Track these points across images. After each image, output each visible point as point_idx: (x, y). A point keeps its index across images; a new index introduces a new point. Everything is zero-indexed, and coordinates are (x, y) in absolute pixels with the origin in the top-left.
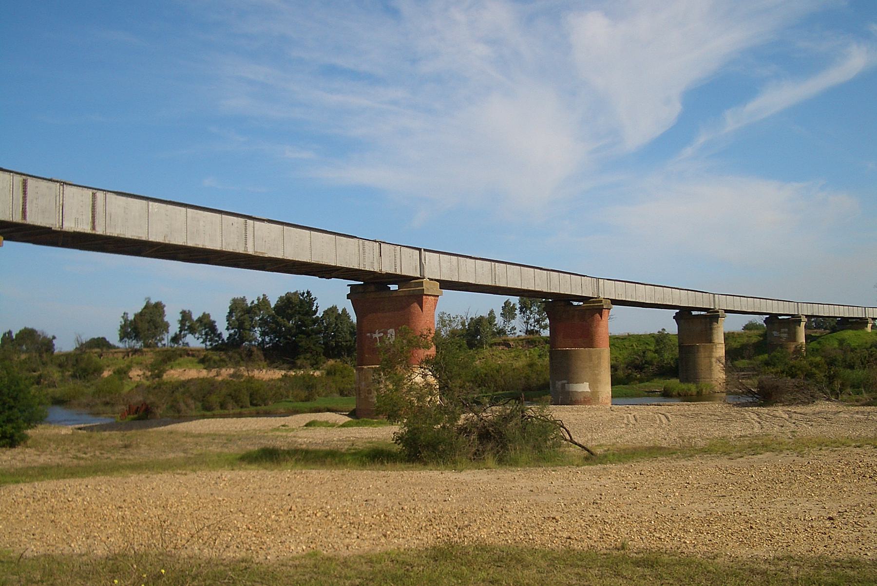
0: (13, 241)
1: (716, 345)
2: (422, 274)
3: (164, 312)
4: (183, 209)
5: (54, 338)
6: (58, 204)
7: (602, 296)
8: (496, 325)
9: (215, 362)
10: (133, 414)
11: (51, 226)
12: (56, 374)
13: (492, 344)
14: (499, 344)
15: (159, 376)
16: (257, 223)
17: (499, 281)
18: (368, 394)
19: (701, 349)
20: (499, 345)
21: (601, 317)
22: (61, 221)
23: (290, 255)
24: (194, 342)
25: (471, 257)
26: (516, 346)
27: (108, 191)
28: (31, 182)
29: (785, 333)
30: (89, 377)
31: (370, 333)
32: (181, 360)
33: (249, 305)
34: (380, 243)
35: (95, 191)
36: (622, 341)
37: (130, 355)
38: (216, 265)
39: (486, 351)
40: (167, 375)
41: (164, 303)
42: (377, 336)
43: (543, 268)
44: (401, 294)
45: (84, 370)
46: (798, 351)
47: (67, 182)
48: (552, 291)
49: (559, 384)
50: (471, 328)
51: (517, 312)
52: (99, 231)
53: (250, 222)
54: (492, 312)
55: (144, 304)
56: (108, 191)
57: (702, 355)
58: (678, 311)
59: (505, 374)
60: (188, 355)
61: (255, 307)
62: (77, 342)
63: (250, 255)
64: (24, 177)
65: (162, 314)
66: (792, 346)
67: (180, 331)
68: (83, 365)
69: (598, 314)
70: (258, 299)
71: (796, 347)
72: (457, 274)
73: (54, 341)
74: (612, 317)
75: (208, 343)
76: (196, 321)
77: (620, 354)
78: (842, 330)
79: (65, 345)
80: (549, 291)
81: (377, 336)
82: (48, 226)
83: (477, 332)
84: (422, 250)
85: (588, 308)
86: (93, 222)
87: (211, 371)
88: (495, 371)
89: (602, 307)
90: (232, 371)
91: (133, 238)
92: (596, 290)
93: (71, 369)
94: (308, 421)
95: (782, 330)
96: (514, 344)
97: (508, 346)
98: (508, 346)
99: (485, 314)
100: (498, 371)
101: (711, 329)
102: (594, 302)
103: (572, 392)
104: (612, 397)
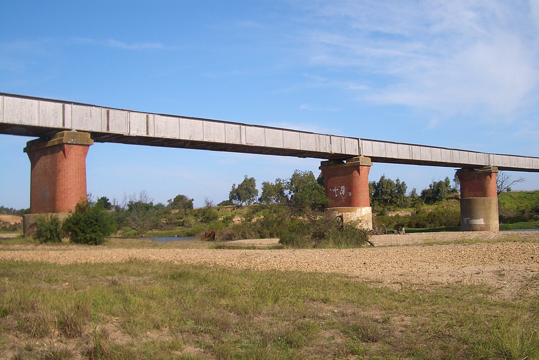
0: (4, 134)
2: (360, 154)
4: (201, 121)
5: (193, 200)
6: (127, 122)
7: (492, 165)
8: (450, 186)
10: (207, 238)
11: (123, 134)
12: (192, 220)
13: (448, 198)
14: (452, 198)
16: (247, 127)
17: (415, 157)
20: (452, 199)
22: (129, 131)
23: (185, 136)
25: (394, 143)
27: (155, 114)
28: (111, 111)
30: (210, 222)
34: (330, 136)
35: (148, 114)
36: (531, 195)
37: (235, 209)
38: (152, 146)
39: (444, 203)
42: (335, 190)
43: (447, 148)
44: (347, 165)
45: (208, 218)
47: (131, 110)
48: (454, 162)
49: (465, 220)
50: (435, 188)
52: (151, 135)
53: (243, 127)
54: (447, 178)
56: (155, 114)
59: (447, 216)
62: (206, 202)
63: (243, 145)
64: (107, 109)
65: (253, 185)
68: (207, 215)
72: (385, 153)
73: (193, 202)
77: (529, 203)
79: (198, 204)
80: (452, 162)
81: (335, 190)
82: (121, 134)
83: (438, 191)
84: (360, 139)
85: (482, 172)
86: (147, 131)
88: (440, 214)
91: (171, 138)
92: (487, 160)
93: (201, 218)
99: (443, 180)
100: (442, 214)
102: (486, 169)
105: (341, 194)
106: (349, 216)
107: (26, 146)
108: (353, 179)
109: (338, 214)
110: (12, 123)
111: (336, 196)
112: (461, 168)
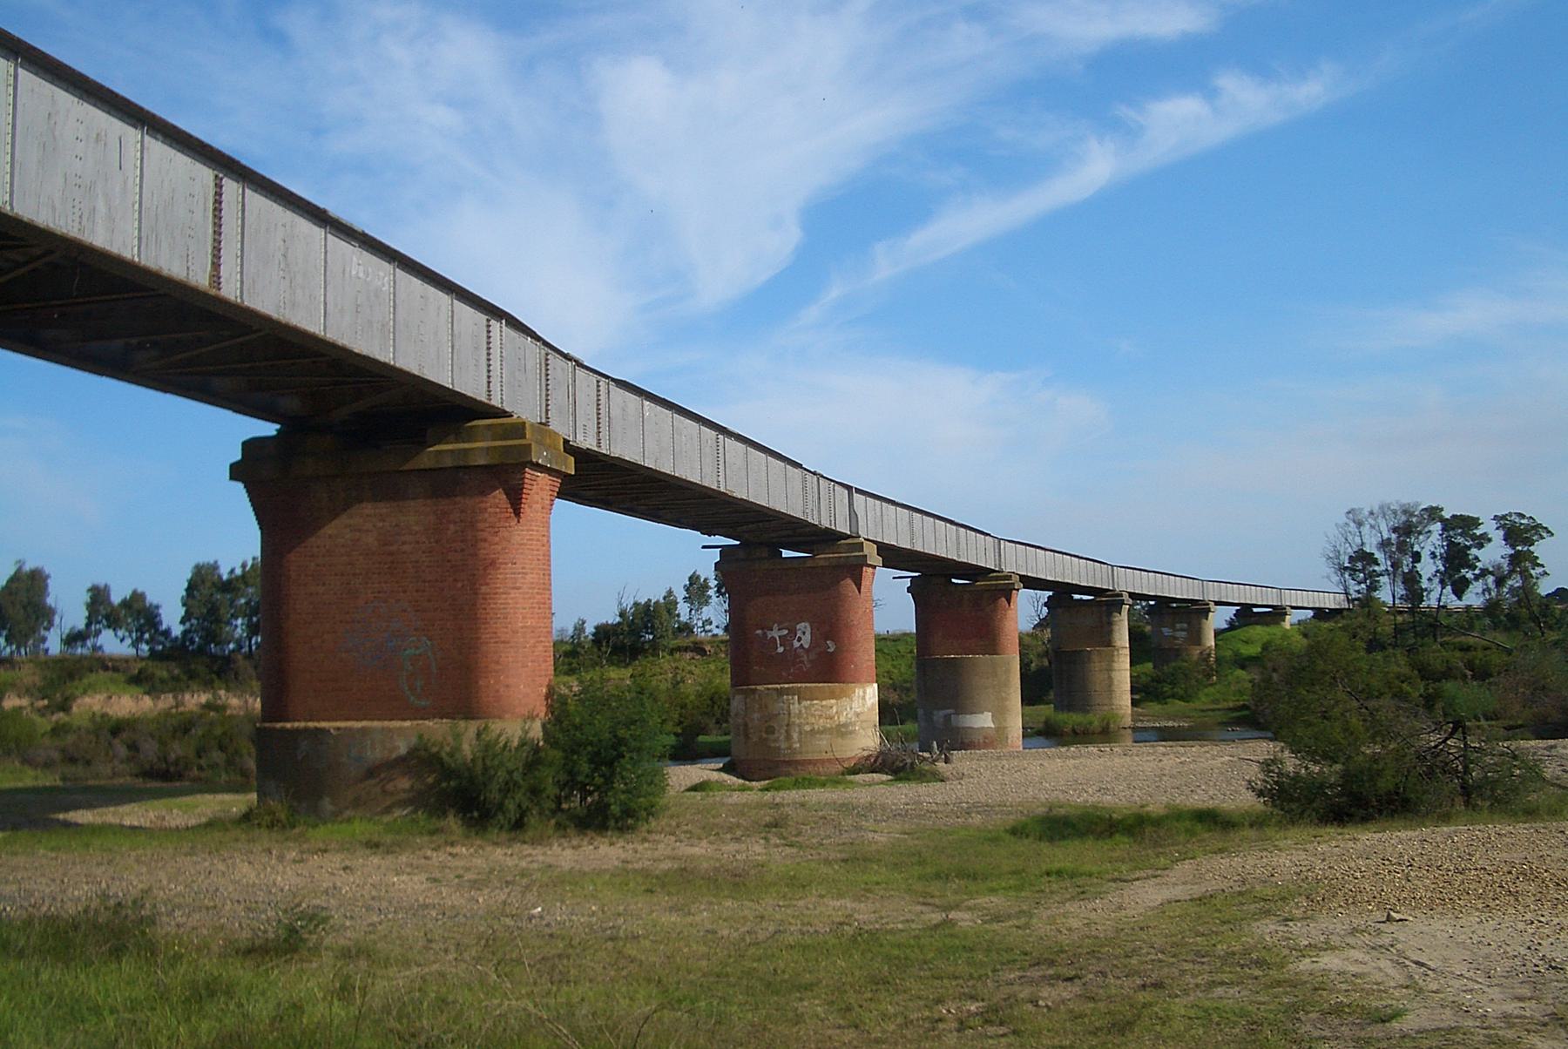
1: (1118, 650)
2: (854, 530)
3: (47, 586)
9: (162, 681)
14: (686, 649)
15: (65, 707)
18: (767, 732)
19: (1095, 657)
21: (1009, 604)
24: (113, 643)
26: (716, 653)
29: (1182, 630)
31: (762, 629)
32: (93, 677)
33: (225, 577)
40: (79, 707)
41: (47, 570)
42: (775, 634)
46: (1205, 657)
51: (711, 592)
54: (670, 592)
55: (12, 572)
57: (1096, 665)
58: (1051, 593)
60: (106, 668)
61: (237, 578)
66: (1196, 651)
67: (88, 625)
69: (1003, 599)
70: (244, 566)
71: (1201, 653)
74: (879, 603)
75: (145, 647)
76: (120, 605)
77: (894, 667)
78: (1245, 626)
81: (775, 634)
87: (159, 698)
89: (1011, 587)
90: (204, 698)
94: (697, 781)
95: (1178, 626)
96: (712, 651)
97: (702, 651)
98: (702, 651)
101: (1110, 624)
102: (997, 578)
103: (963, 728)
104: (1023, 737)
105: (796, 644)
106: (834, 710)
107: (239, 457)
108: (840, 603)
109: (799, 703)
110: (408, 370)
111: (781, 650)
112: (917, 574)
